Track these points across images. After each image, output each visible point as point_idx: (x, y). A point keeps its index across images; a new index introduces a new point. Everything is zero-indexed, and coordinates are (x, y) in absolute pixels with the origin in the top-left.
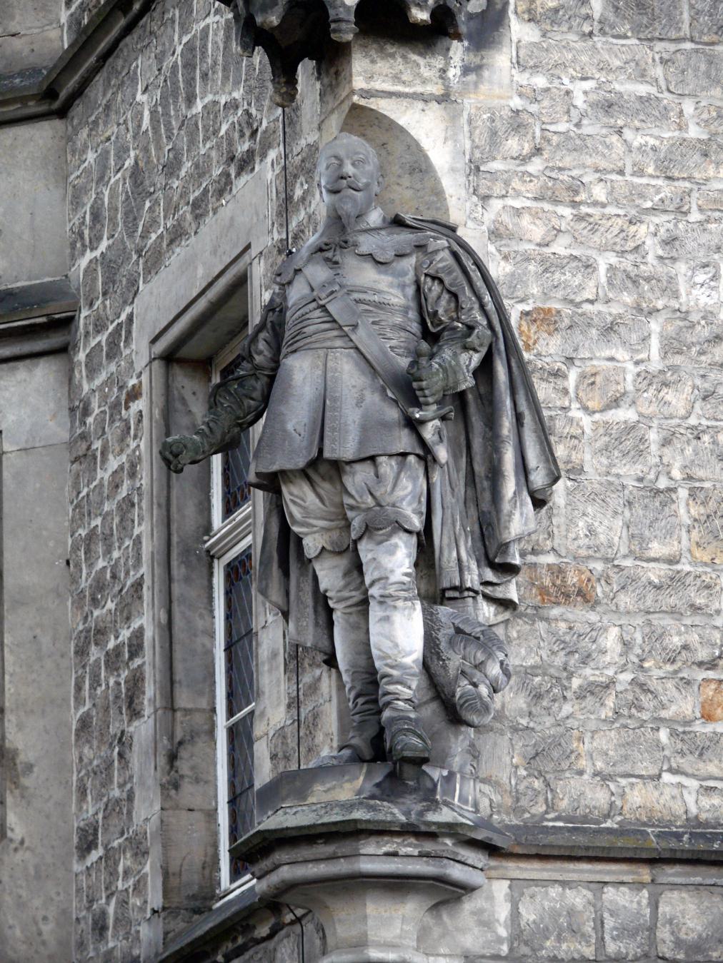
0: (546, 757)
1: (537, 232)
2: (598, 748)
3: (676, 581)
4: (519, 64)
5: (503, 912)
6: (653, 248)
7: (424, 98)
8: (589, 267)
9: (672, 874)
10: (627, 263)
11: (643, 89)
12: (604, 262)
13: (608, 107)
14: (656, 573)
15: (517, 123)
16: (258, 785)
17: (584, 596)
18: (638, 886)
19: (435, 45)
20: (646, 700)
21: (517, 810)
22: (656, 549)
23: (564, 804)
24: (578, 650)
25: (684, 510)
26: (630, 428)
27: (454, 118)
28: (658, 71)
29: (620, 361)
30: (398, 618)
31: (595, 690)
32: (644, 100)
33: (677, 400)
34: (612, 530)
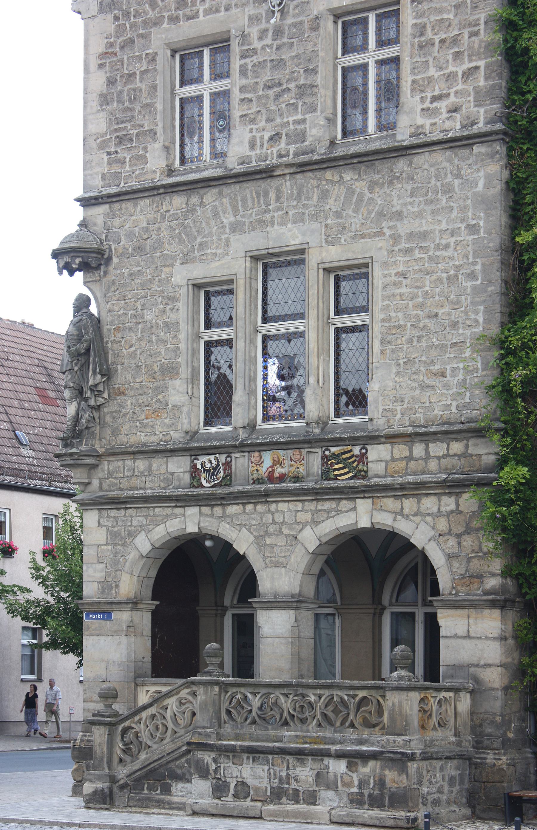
0: (116, 432)
1: (117, 309)
2: (126, 427)
3: (142, 387)
4: (115, 269)
5: (106, 468)
6: (140, 307)
7: (96, 281)
8: (126, 315)
9: (138, 456)
10: (134, 312)
11: (139, 269)
12: (130, 313)
13: (131, 275)
14: (138, 386)
15: (114, 283)
16: (215, 560)
17: (124, 394)
18: (131, 459)
19: (76, 300)
20: (135, 416)
21: (110, 444)
22: (138, 380)
23: (118, 442)
24: (122, 406)
25: (143, 370)
26: (134, 352)
27: (101, 285)
28: (142, 264)
29: (132, 337)
30: (316, 414)
31: (125, 415)
32: (139, 271)
33: (143, 343)
34: (129, 377)
